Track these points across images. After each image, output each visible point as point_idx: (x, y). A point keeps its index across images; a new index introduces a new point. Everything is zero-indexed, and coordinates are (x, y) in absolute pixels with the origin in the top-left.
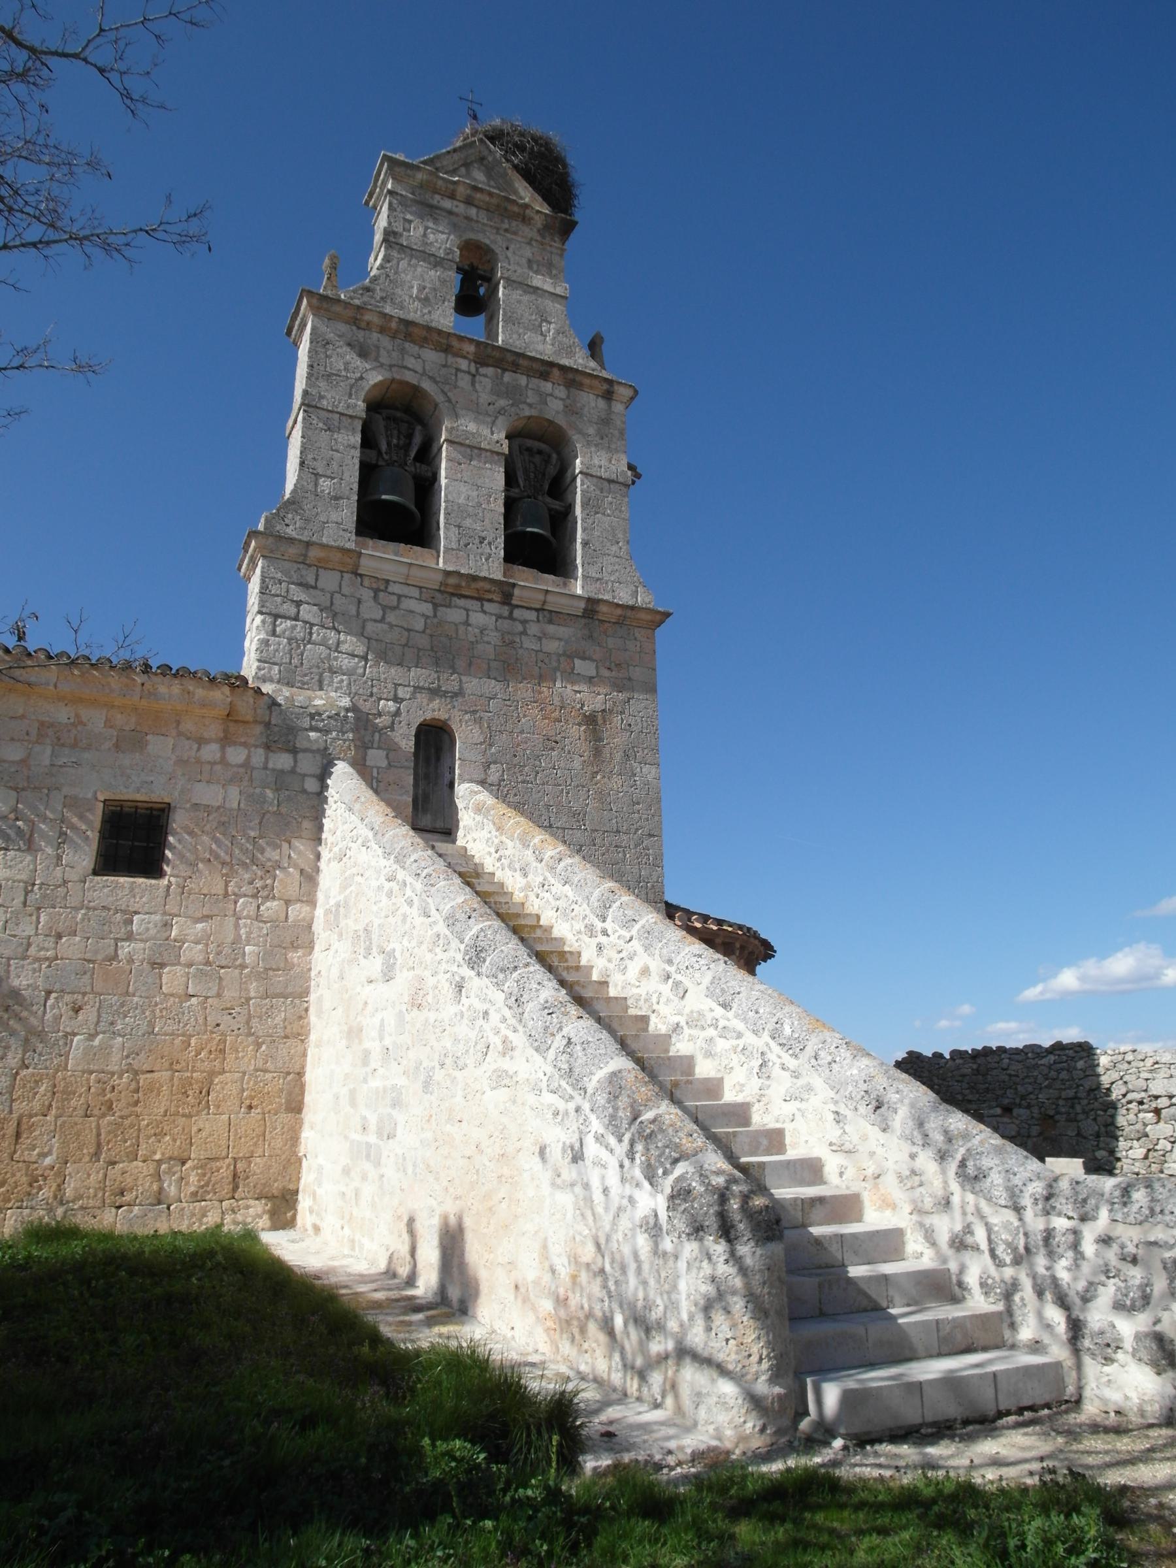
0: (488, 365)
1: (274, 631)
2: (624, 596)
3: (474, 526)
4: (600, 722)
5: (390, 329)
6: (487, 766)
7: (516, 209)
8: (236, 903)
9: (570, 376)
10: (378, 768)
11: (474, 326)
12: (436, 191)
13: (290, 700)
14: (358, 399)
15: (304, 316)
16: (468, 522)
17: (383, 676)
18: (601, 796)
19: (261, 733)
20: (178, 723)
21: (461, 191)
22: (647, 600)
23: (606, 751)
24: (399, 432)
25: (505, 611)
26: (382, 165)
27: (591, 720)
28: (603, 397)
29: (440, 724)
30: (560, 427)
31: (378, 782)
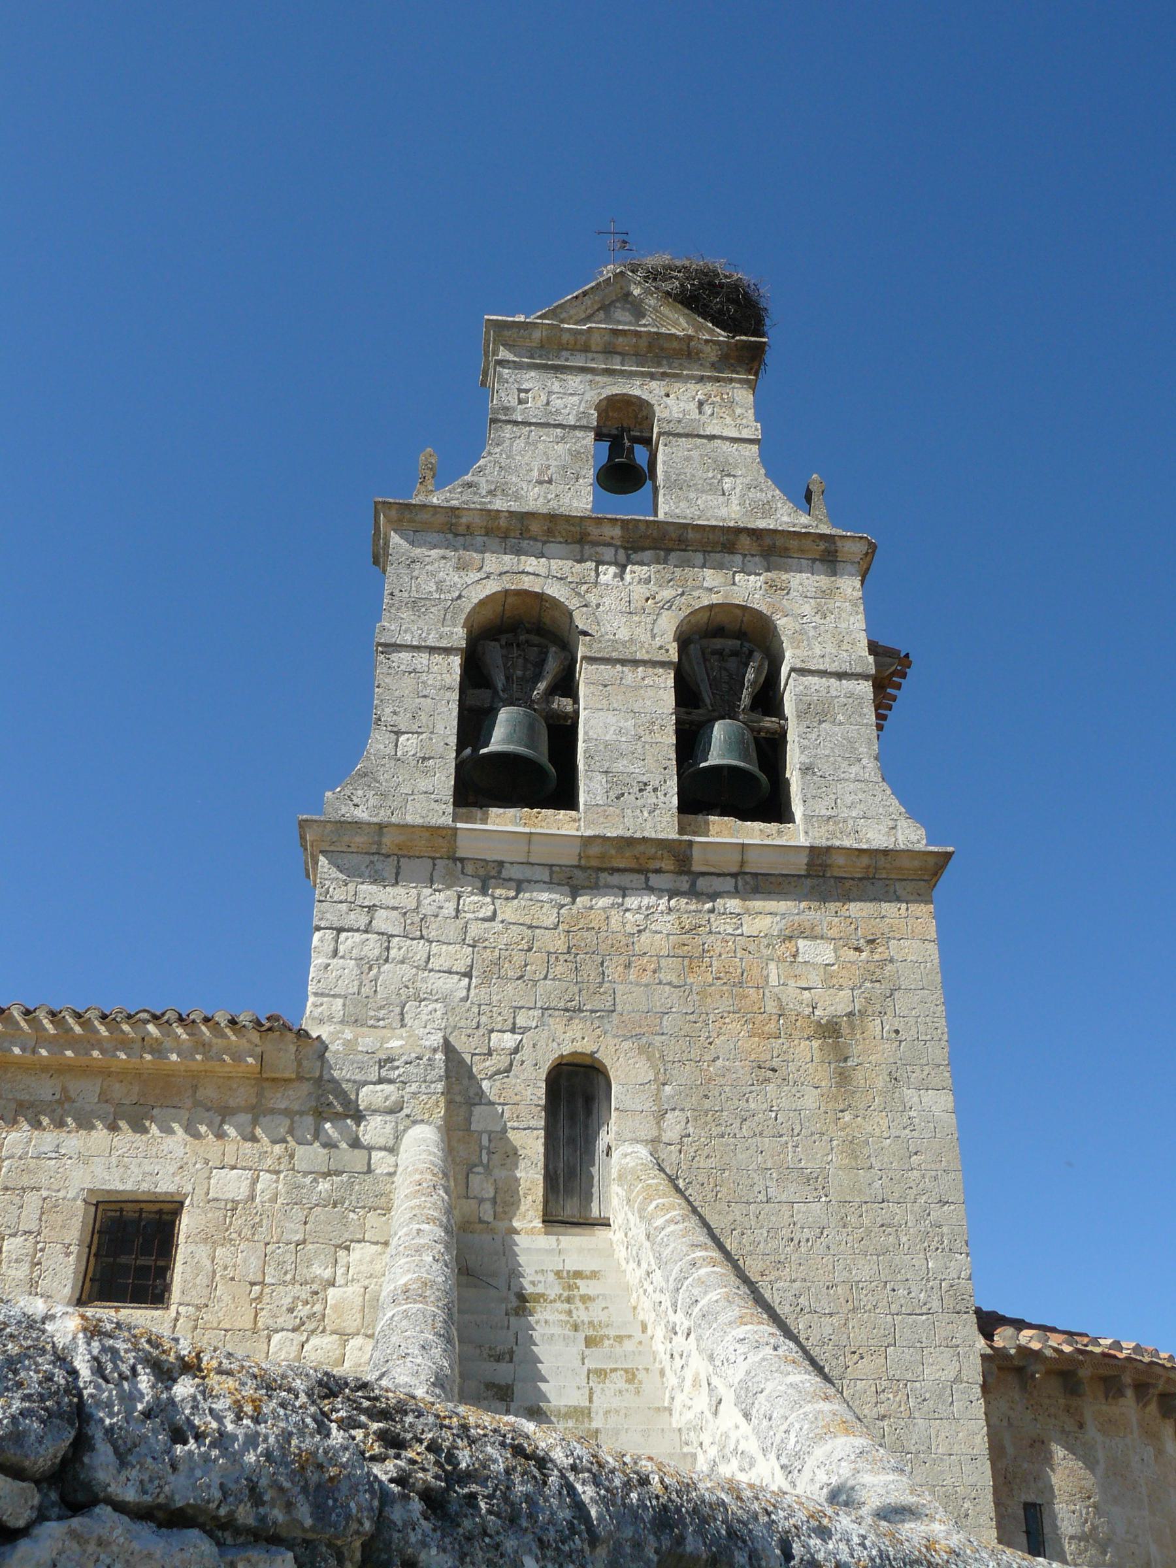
0: (643, 549)
1: (335, 953)
2: (875, 837)
3: (631, 769)
4: (845, 1030)
5: (499, 528)
6: (661, 1115)
7: (675, 345)
8: (269, 1339)
9: (768, 541)
10: (490, 1133)
11: (627, 507)
12: (563, 347)
13: (350, 1045)
14: (455, 625)
15: (385, 534)
16: (619, 766)
17: (495, 998)
18: (853, 1147)
19: (310, 1094)
20: (195, 1088)
21: (596, 341)
22: (914, 838)
23: (859, 1077)
24: (526, 660)
25: (684, 883)
26: (488, 333)
27: (830, 1031)
28: (822, 561)
29: (588, 1061)
30: (759, 613)
31: (490, 1153)
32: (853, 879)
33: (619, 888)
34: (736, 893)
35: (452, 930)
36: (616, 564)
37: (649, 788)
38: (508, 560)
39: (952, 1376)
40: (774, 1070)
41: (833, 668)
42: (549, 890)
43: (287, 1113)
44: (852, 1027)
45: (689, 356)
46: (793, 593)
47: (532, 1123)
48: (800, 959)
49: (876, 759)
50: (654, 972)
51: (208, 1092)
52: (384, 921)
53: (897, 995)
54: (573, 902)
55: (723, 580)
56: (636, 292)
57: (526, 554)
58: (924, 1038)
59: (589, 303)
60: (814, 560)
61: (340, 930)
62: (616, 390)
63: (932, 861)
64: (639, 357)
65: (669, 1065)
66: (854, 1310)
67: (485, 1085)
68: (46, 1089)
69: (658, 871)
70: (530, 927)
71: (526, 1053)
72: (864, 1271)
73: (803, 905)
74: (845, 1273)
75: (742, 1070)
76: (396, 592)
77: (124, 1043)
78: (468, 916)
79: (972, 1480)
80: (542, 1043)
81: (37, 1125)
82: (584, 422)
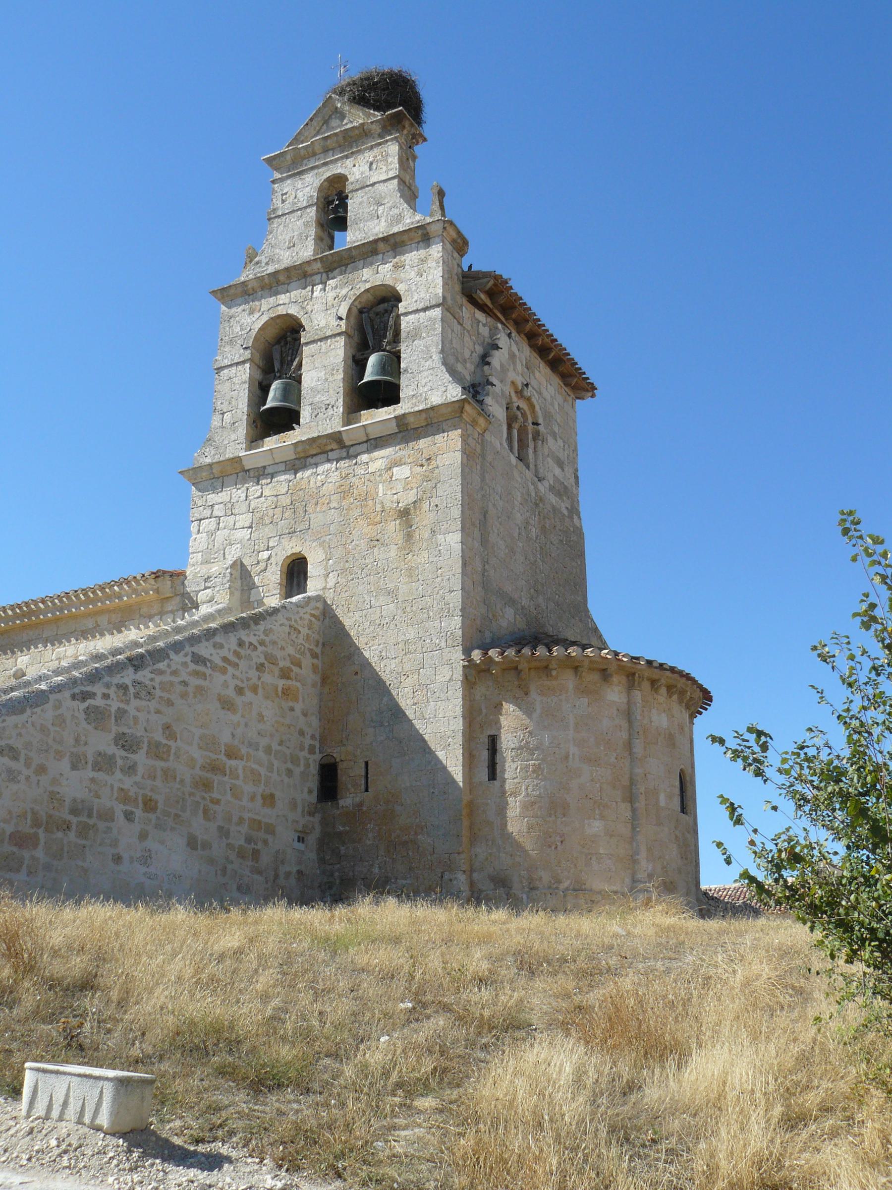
7: (357, 132)
9: (392, 241)
21: (318, 148)
22: (455, 394)
23: (416, 536)
28: (423, 241)
32: (422, 427)
33: (315, 464)
34: (368, 451)
35: (244, 508)
36: (321, 283)
37: (330, 407)
38: (272, 300)
39: (448, 678)
40: (378, 540)
41: (421, 306)
42: (285, 474)
43: (172, 612)
44: (415, 508)
45: (366, 135)
46: (407, 267)
47: (275, 592)
48: (394, 479)
49: (440, 353)
50: (328, 504)
51: (144, 610)
52: (218, 511)
53: (438, 485)
54: (295, 478)
55: (371, 273)
56: (339, 105)
57: (280, 293)
58: (449, 505)
59: (315, 124)
60: (418, 242)
61: (200, 520)
62: (328, 174)
63: (457, 406)
64: (341, 147)
65: (332, 550)
66: (405, 654)
67: (256, 579)
68: (90, 623)
69: (332, 450)
70: (276, 496)
71: (273, 560)
72: (411, 634)
73: (398, 448)
74: (403, 637)
75: (363, 544)
76: (224, 338)
77: (109, 597)
78: (252, 497)
79: (453, 728)
80: (279, 553)
81: (86, 638)
82: (310, 203)
